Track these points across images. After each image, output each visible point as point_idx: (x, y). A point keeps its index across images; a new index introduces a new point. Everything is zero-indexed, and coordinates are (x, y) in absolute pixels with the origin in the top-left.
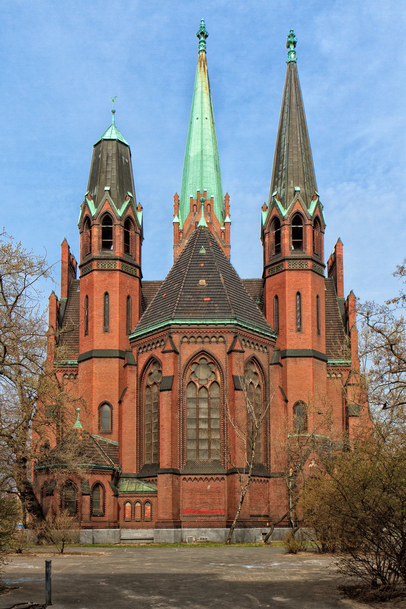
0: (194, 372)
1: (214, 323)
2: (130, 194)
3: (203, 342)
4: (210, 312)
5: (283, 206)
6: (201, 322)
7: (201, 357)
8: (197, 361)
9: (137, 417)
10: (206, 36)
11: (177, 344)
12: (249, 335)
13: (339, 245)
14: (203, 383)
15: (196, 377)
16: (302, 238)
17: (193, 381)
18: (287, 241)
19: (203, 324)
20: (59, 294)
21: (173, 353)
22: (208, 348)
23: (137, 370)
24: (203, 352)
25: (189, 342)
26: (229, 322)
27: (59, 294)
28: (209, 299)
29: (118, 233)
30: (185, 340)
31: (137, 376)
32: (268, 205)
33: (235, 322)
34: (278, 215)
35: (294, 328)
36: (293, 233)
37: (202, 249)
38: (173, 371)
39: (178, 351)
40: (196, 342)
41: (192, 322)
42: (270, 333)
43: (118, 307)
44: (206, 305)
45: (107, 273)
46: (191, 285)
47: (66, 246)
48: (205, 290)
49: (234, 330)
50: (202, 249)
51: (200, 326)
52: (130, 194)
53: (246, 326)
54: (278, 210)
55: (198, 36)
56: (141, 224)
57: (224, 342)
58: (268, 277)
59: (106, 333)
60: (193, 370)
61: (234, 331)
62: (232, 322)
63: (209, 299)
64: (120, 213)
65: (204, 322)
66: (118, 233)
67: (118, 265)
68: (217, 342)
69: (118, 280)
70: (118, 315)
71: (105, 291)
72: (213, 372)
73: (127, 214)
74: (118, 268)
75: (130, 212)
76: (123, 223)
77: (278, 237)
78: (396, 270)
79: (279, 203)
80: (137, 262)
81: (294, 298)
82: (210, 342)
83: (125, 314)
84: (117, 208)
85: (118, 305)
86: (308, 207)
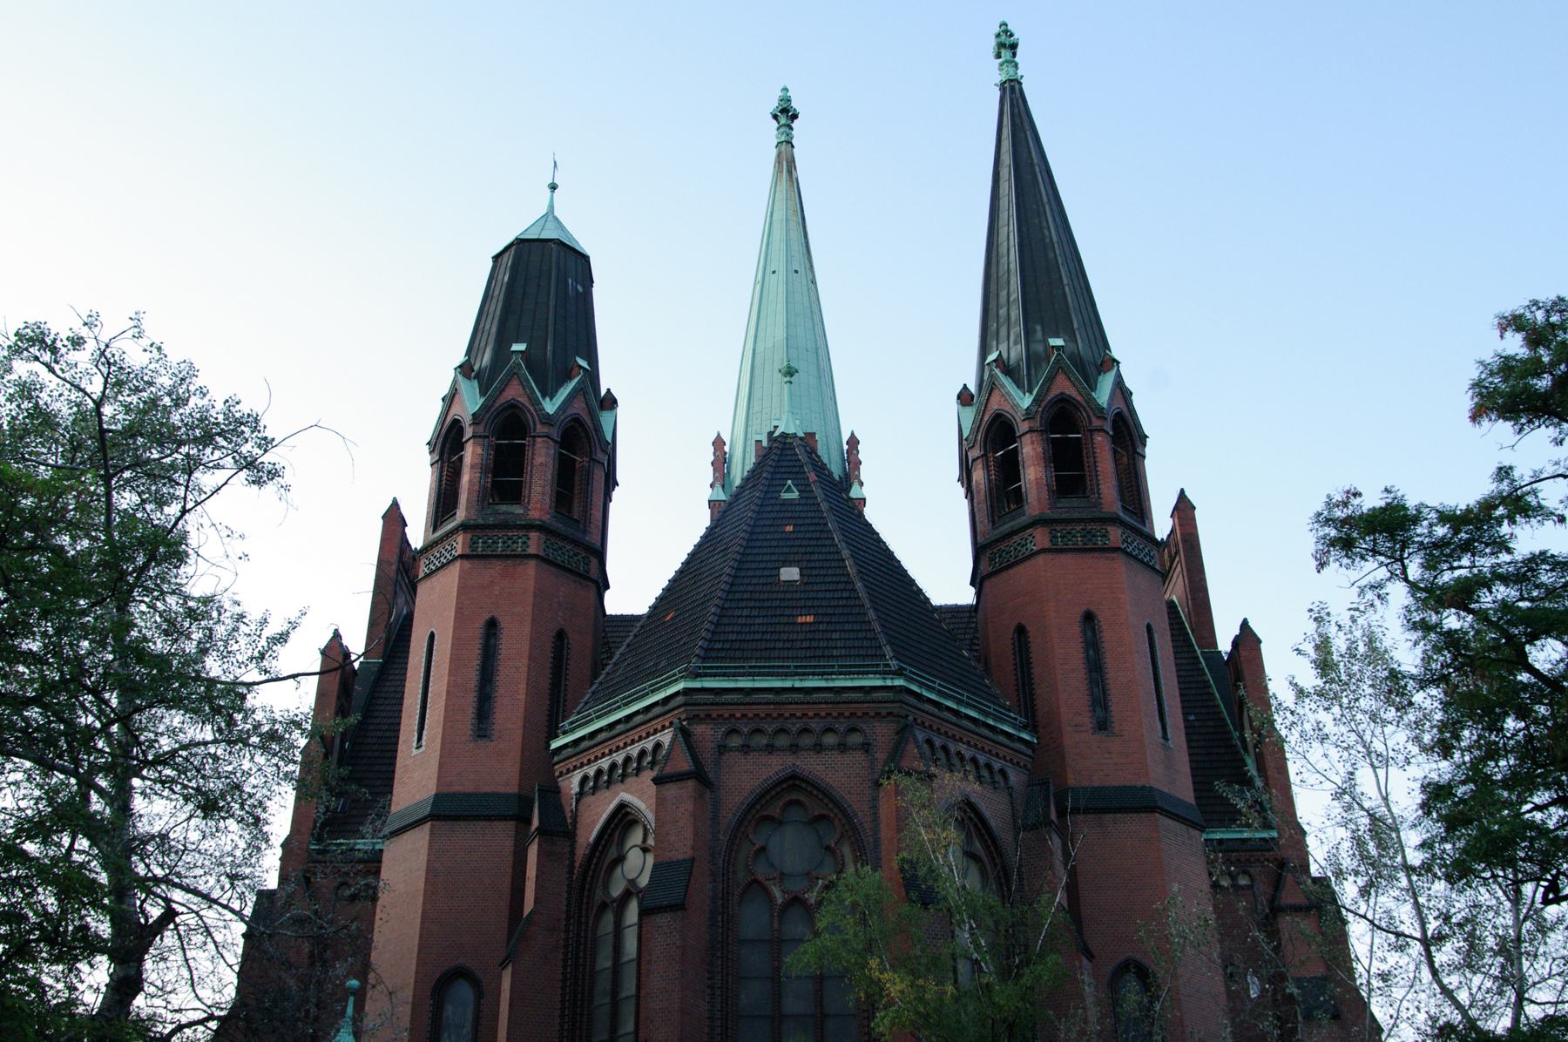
0: (763, 849)
1: (831, 684)
2: (584, 363)
3: (794, 749)
4: (814, 655)
5: (1019, 384)
6: (788, 684)
7: (787, 798)
8: (775, 810)
9: (562, 1016)
10: (795, 117)
11: (707, 756)
12: (945, 727)
13: (1184, 509)
14: (796, 886)
15: (772, 865)
16: (1082, 469)
17: (761, 878)
18: (1033, 474)
19: (793, 690)
20: (356, 643)
21: (691, 784)
22: (811, 765)
23: (572, 853)
24: (793, 781)
25: (746, 749)
26: (879, 683)
27: (356, 643)
28: (810, 619)
29: (542, 458)
30: (736, 741)
31: (571, 872)
32: (972, 388)
33: (899, 682)
34: (1008, 408)
35: (1086, 720)
36: (1057, 439)
37: (791, 496)
38: (690, 843)
39: (711, 776)
40: (770, 749)
41: (757, 685)
42: (1014, 726)
43: (525, 661)
44: (801, 636)
45: (497, 567)
46: (755, 581)
47: (394, 519)
48: (798, 596)
49: (895, 708)
50: (791, 496)
51: (785, 697)
52: (584, 363)
53: (933, 697)
54: (1006, 396)
55: (775, 117)
56: (609, 439)
57: (866, 747)
58: (990, 575)
59: (481, 742)
60: (759, 844)
61: (896, 711)
62: (889, 683)
63: (810, 619)
64: (550, 407)
65: (798, 684)
66: (542, 458)
67: (535, 543)
68: (842, 748)
69: (530, 585)
70: (523, 686)
71: (488, 616)
72: (828, 848)
73: (571, 411)
74: (532, 550)
75: (578, 408)
76: (555, 433)
77: (1009, 469)
78: (1498, 333)
79: (1007, 382)
80: (594, 539)
81: (1077, 629)
82: (819, 748)
83: (545, 683)
84: (544, 397)
85: (526, 655)
86: (1094, 388)
